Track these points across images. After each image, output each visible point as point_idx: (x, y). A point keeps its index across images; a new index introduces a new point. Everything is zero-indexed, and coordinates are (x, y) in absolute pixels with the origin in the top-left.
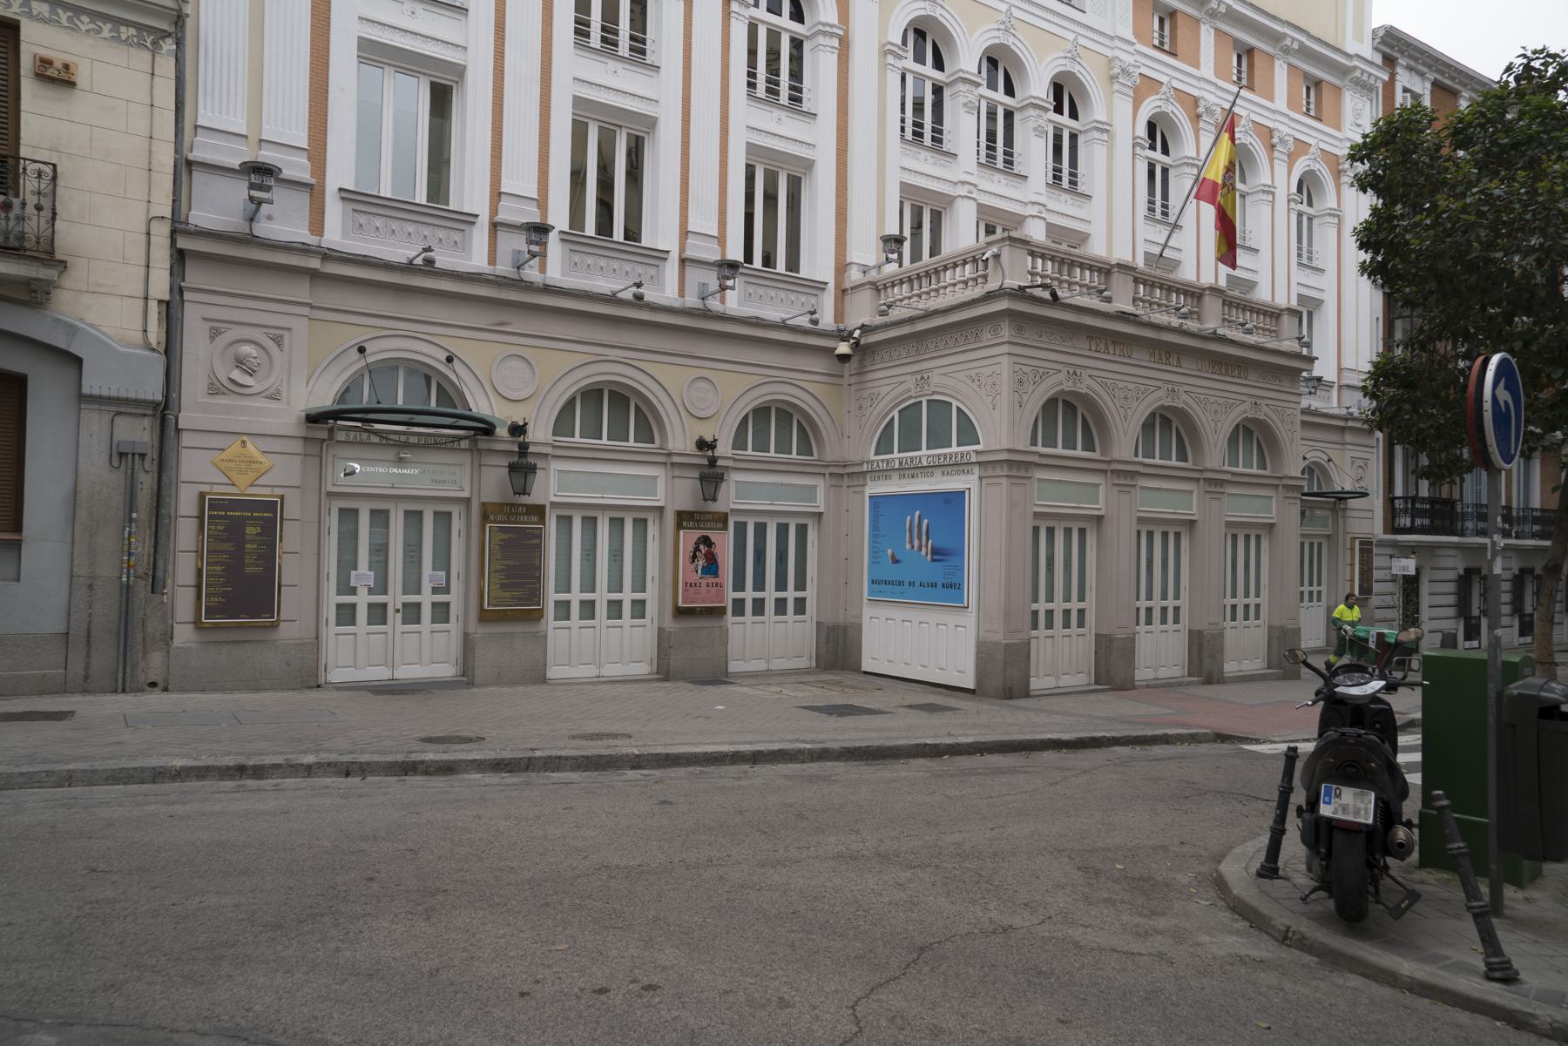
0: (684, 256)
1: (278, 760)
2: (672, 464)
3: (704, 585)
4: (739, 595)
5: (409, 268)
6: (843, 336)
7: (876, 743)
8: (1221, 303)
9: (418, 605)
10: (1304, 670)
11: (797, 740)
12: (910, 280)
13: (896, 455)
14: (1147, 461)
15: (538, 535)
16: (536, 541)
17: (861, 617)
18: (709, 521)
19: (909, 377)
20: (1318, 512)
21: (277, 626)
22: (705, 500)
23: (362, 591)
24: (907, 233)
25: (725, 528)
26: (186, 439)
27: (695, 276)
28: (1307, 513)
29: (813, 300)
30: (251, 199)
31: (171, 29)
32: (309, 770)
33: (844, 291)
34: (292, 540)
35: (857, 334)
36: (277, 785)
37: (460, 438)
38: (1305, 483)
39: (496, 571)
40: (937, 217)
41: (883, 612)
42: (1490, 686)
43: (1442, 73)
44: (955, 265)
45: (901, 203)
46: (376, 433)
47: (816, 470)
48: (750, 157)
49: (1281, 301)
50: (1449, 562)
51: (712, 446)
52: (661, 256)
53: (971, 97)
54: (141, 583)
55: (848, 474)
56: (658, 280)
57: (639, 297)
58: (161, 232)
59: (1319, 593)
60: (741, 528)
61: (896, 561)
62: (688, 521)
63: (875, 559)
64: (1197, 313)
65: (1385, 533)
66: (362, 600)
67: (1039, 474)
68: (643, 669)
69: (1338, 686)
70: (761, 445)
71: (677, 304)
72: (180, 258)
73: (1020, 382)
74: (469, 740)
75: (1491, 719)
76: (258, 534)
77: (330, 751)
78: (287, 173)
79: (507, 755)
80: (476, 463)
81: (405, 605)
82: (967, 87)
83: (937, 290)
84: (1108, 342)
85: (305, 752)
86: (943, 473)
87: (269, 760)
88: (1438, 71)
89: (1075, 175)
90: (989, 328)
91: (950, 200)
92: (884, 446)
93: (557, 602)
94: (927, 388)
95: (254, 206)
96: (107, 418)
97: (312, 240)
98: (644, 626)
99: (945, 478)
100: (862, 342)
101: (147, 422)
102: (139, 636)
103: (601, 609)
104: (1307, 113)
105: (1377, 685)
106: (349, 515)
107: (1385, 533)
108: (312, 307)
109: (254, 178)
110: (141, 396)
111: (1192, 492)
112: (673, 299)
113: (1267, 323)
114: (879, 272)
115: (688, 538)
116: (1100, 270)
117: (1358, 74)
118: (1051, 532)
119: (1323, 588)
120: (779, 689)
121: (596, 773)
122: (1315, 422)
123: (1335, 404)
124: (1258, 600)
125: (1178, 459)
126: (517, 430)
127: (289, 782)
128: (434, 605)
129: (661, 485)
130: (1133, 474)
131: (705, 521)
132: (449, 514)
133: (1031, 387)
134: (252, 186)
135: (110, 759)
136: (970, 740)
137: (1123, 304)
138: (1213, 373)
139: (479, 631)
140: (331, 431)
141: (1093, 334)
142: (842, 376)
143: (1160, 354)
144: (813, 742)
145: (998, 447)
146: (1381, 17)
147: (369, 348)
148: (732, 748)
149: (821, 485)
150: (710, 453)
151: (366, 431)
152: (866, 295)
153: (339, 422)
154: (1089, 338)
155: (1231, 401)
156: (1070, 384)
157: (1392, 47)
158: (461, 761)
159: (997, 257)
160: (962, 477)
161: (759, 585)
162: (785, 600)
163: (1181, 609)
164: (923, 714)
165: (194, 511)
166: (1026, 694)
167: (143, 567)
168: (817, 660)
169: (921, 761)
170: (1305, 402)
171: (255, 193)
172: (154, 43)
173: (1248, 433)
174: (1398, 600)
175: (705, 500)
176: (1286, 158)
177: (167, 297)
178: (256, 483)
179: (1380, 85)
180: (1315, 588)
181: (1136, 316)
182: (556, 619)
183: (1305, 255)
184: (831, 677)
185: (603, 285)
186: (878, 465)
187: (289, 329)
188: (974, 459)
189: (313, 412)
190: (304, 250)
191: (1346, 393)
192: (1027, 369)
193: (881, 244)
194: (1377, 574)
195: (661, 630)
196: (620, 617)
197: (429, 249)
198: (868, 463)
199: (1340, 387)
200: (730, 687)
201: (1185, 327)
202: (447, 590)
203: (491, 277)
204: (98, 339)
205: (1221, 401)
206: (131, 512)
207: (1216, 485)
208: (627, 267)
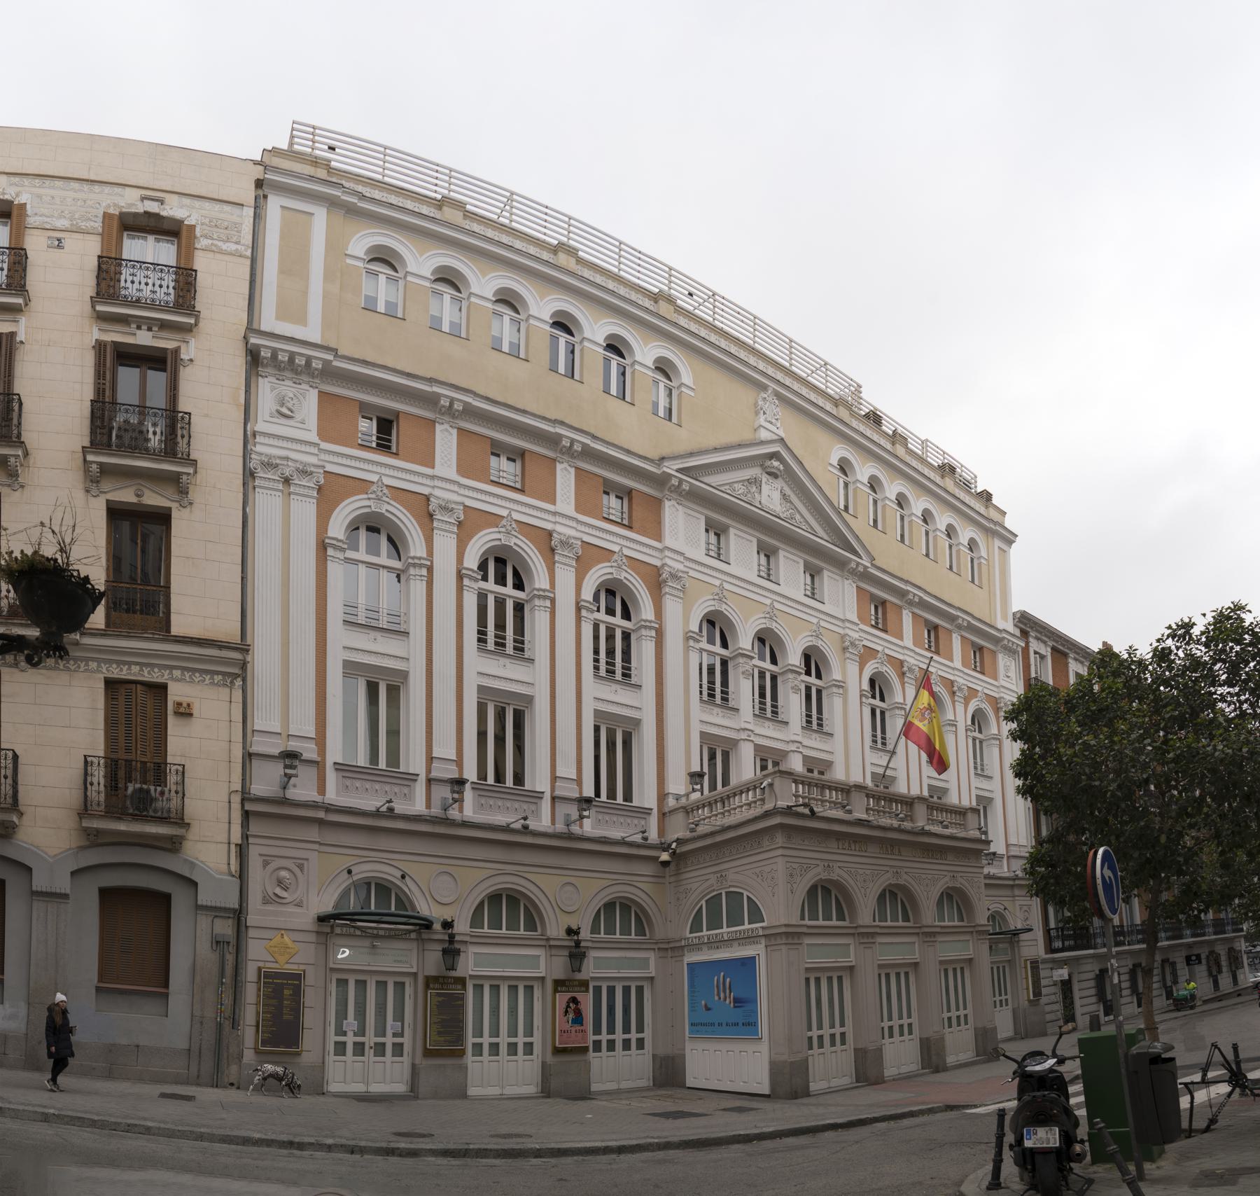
1: (312, 1140)
2: (550, 946)
3: (573, 1032)
4: (597, 1038)
5: (377, 814)
6: (665, 847)
7: (704, 1136)
8: (926, 809)
9: (384, 1044)
10: (1002, 1058)
11: (647, 1137)
12: (710, 804)
13: (705, 933)
15: (462, 998)
16: (460, 1002)
17: (684, 1049)
18: (576, 986)
19: (712, 875)
20: (1001, 946)
21: (300, 1055)
22: (573, 971)
23: (350, 1034)
24: (706, 769)
25: (587, 991)
26: (251, 933)
27: (563, 809)
28: (994, 947)
29: (643, 822)
30: (286, 775)
31: (240, 672)
32: (329, 1148)
33: (664, 814)
34: (310, 998)
35: (674, 846)
36: (311, 1155)
37: (410, 932)
38: (990, 928)
39: (435, 1023)
40: (726, 756)
41: (700, 1045)
42: (1120, 1051)
43: (1057, 642)
44: (742, 792)
45: (701, 746)
46: (358, 928)
47: (648, 946)
49: (966, 803)
50: (1089, 967)
51: (577, 933)
52: (538, 796)
53: (748, 667)
54: (227, 1022)
55: (671, 948)
56: (537, 813)
57: (526, 827)
58: (237, 799)
59: (1006, 1000)
60: (598, 990)
61: (708, 1009)
62: (562, 986)
63: (692, 1008)
64: (910, 816)
65: (1046, 953)
66: (350, 1039)
67: (807, 941)
68: (532, 1090)
69: (1027, 1066)
70: (610, 930)
71: (550, 830)
72: (246, 815)
73: (791, 875)
74: (424, 1136)
75: (1123, 1071)
76: (290, 995)
77: (341, 1137)
78: (306, 756)
79: (451, 1146)
81: (376, 1044)
82: (745, 659)
83: (729, 811)
85: (326, 1137)
86: (739, 944)
87: (307, 1140)
88: (1054, 640)
89: (776, 707)
90: (767, 837)
91: (735, 743)
92: (696, 927)
94: (725, 883)
95: (286, 779)
96: (210, 919)
97: (318, 798)
99: (740, 947)
100: (678, 851)
101: (230, 922)
102: (225, 1055)
103: (503, 1049)
104: (975, 670)
105: (1052, 1062)
106: (343, 983)
107: (1046, 953)
108: (320, 844)
109: (288, 762)
110: (228, 906)
111: (914, 943)
112: (548, 827)
113: (957, 819)
114: (688, 799)
115: (562, 999)
116: (842, 790)
117: (1006, 642)
118: (818, 980)
119: (1009, 997)
120: (628, 1102)
121: (511, 1160)
122: (994, 884)
123: (1006, 870)
124: (965, 1012)
125: (903, 921)
126: (447, 925)
127: (318, 1154)
128: (394, 1044)
130: (873, 935)
132: (403, 984)
134: (286, 767)
135: (220, 1128)
136: (771, 1129)
140: (332, 927)
141: (840, 836)
142: (664, 877)
143: (886, 848)
144: (658, 1137)
145: (778, 924)
146: (1017, 605)
147: (354, 870)
148: (604, 1144)
149: (652, 956)
150: (576, 938)
151: (353, 927)
152: (680, 818)
153: (337, 921)
154: (838, 840)
155: (936, 876)
157: (1025, 625)
158: (422, 1149)
159: (771, 785)
160: (753, 946)
161: (611, 1030)
162: (630, 1040)
164: (735, 1115)
165: (255, 979)
166: (807, 1094)
167: (228, 1013)
168: (653, 1081)
169: (737, 1146)
170: (986, 871)
171: (288, 771)
172: (232, 682)
173: (950, 897)
174: (1059, 997)
175: (573, 971)
176: (962, 701)
177: (240, 842)
178: (290, 961)
179: (1020, 649)
180: (1003, 997)
181: (869, 821)
182: (473, 1055)
183: (979, 768)
184: (664, 1092)
185: (500, 819)
187: (307, 859)
188: (761, 933)
189: (321, 915)
190: (314, 806)
191: (1013, 861)
192: (795, 866)
193: (688, 778)
194: (1043, 982)
195: (544, 1064)
196: (516, 1054)
197: (390, 801)
198: (685, 939)
199: (1008, 857)
200: (593, 1101)
201: (903, 827)
202: (402, 1035)
203: (428, 818)
204: (205, 870)
206: (222, 978)
207: (930, 937)
208: (517, 805)
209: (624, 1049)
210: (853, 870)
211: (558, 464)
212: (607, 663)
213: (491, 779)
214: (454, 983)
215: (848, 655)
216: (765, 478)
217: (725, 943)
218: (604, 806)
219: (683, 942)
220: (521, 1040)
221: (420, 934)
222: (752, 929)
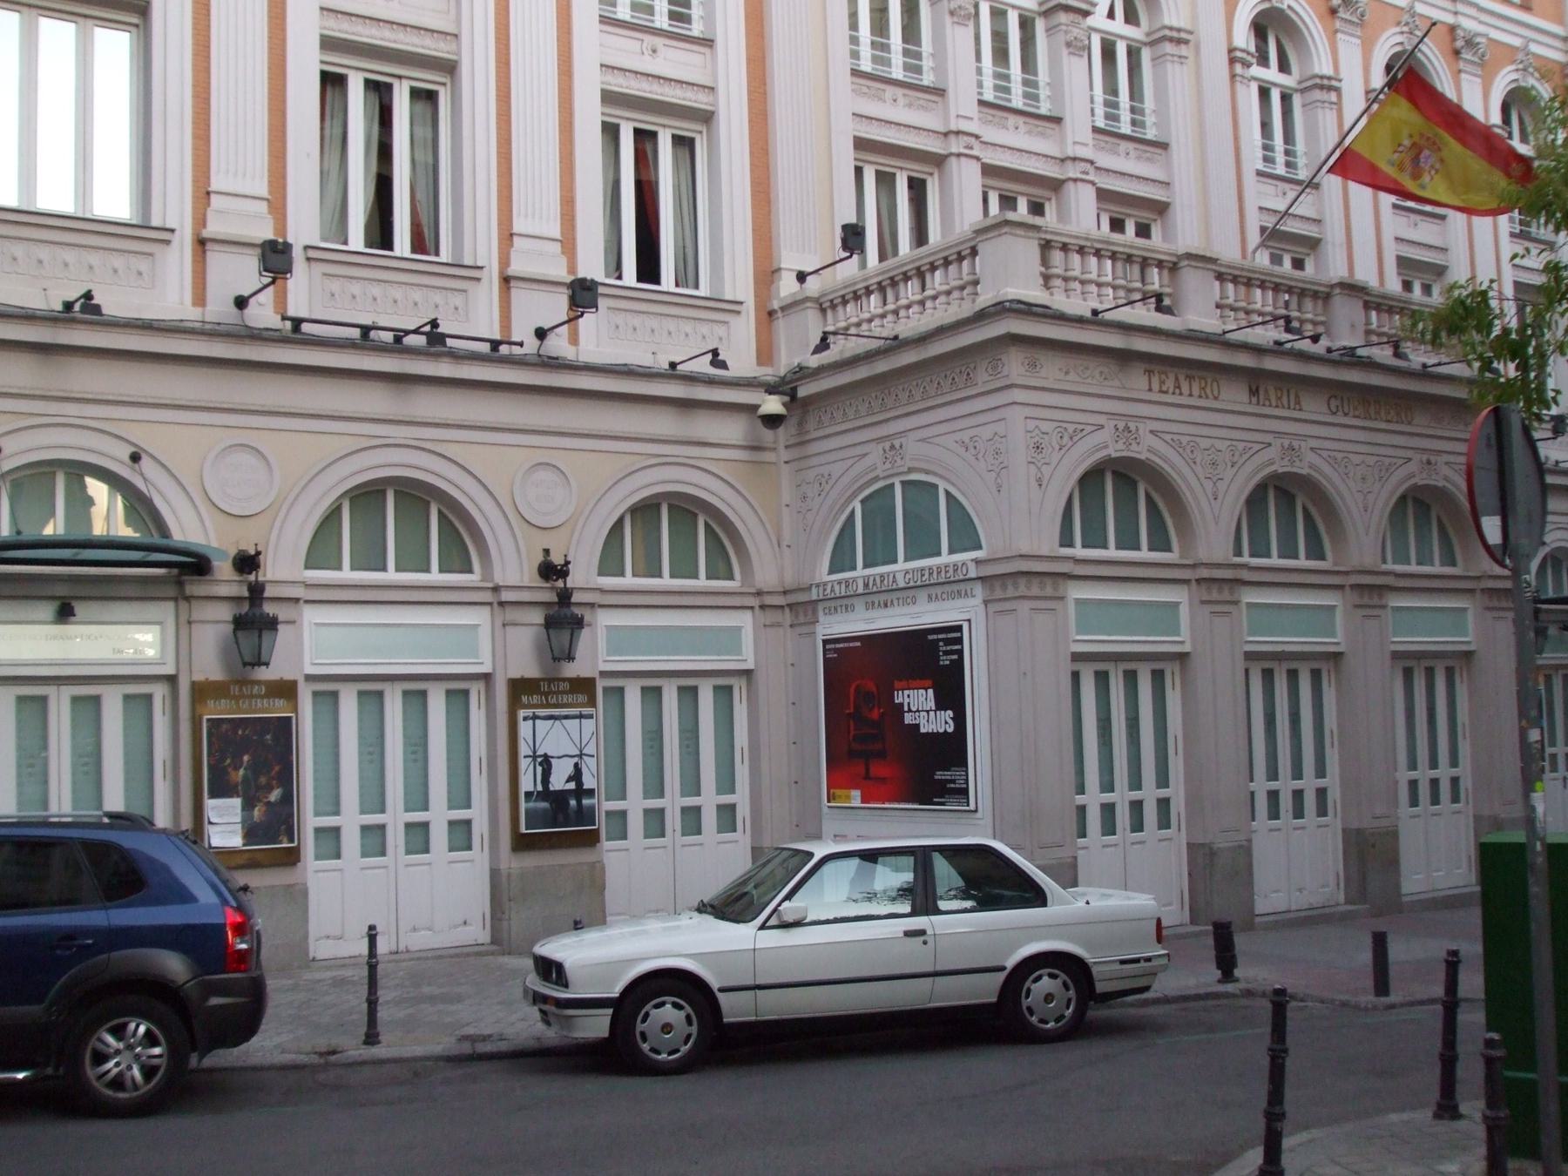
0: (206, 234)
14: (1400, 568)
19: (873, 445)
25: (592, 702)
29: (720, 330)
33: (771, 313)
48: (608, 110)
62: (531, 693)
66: (439, 815)
80: (183, 618)
84: (1181, 378)
86: (930, 597)
92: (842, 559)
93: (318, 831)
94: (899, 462)
98: (472, 861)
103: (396, 838)
126: (247, 563)
131: (558, 693)
133: (1056, 457)
137: (1346, 338)
138: (1355, 417)
139: (514, 863)
149: (479, 618)
155: (1387, 461)
156: (1120, 446)
160: (959, 602)
182: (317, 858)
186: (832, 590)
188: (972, 574)
192: (1045, 426)
195: (495, 874)
198: (818, 586)
205: (1371, 460)
210: (1185, 440)
212: (906, 53)
213: (357, 238)
214: (572, 691)
215: (1462, 65)
217: (899, 594)
218: (626, 294)
219: (814, 590)
220: (1150, 794)
221: (180, 584)
222: (956, 567)
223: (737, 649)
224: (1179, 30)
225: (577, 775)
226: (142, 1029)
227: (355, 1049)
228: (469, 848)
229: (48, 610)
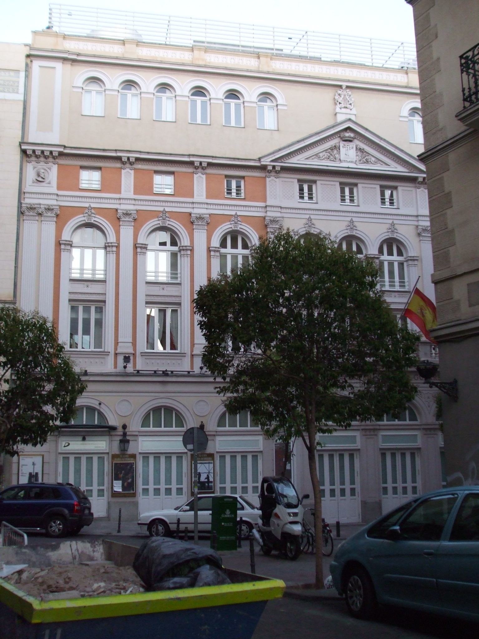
18: (205, 457)
47: (418, 427)
66: (174, 486)
98: (355, 499)
106: (66, 460)
126: (124, 427)
129: (358, 439)
163: (97, 495)
209: (331, 496)
211: (195, 175)
216: (342, 144)
221: (110, 432)
223: (355, 443)
224: (413, 257)
225: (208, 478)
226: (58, 522)
227: (115, 533)
228: (182, 495)
229: (81, 438)
